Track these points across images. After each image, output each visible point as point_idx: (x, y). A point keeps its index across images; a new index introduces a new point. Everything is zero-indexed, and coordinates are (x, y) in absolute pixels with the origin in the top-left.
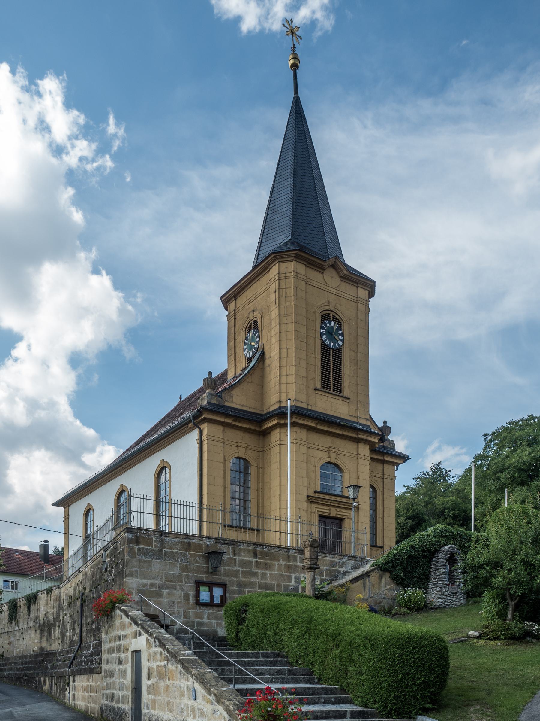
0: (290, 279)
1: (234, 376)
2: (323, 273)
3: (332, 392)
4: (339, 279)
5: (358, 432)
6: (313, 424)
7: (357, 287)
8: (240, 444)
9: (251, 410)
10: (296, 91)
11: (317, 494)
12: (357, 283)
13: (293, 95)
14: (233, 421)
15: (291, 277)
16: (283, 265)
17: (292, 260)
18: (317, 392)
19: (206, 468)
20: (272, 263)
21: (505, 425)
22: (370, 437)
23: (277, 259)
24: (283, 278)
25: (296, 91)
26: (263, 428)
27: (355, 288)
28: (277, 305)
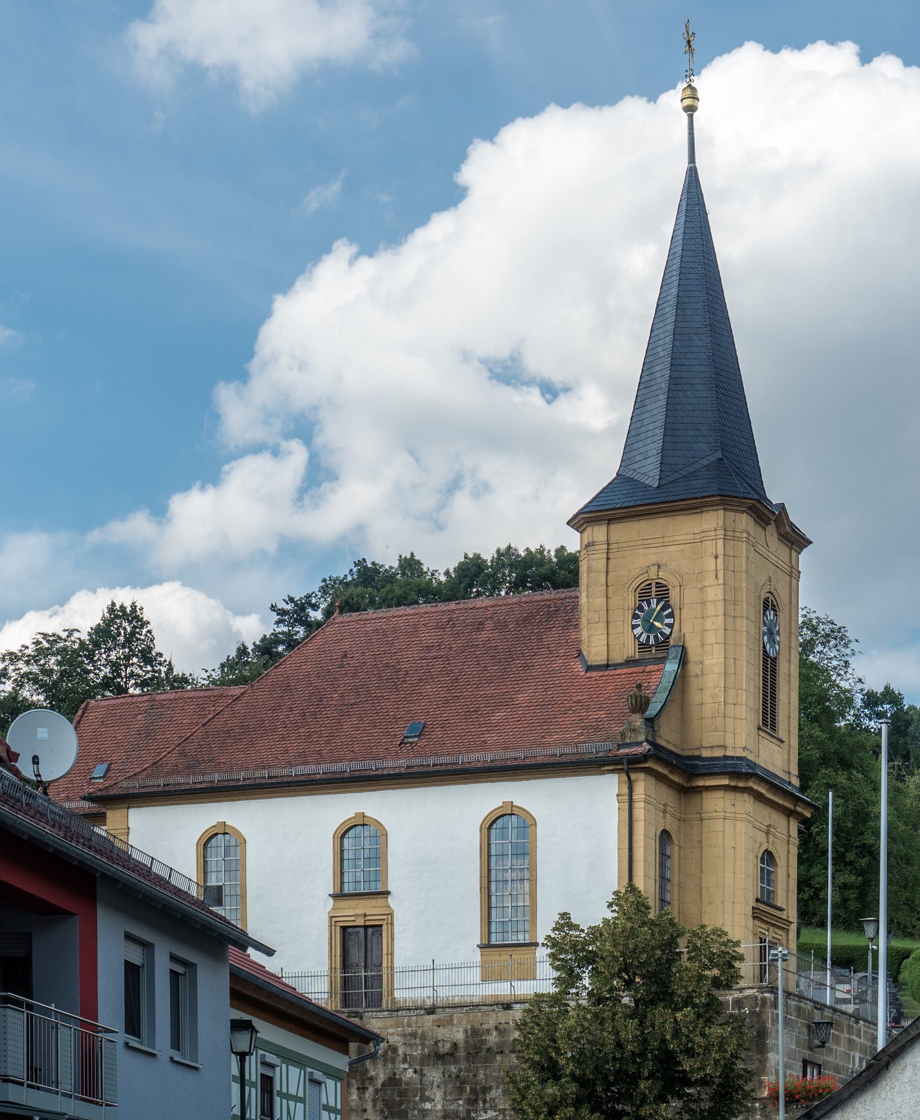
0: (740, 543)
1: (585, 653)
2: (765, 529)
3: (769, 731)
4: (776, 536)
5: (797, 802)
6: (762, 790)
7: (791, 549)
8: (668, 808)
9: (673, 749)
10: (692, 158)
11: (759, 904)
12: (792, 544)
13: (685, 165)
14: (670, 772)
15: (741, 539)
16: (731, 515)
17: (743, 512)
18: (761, 733)
19: (642, 849)
20: (711, 506)
21: (488, 555)
22: (805, 809)
23: (724, 504)
24: (729, 538)
25: (692, 158)
26: (694, 784)
27: (788, 550)
28: (721, 581)
